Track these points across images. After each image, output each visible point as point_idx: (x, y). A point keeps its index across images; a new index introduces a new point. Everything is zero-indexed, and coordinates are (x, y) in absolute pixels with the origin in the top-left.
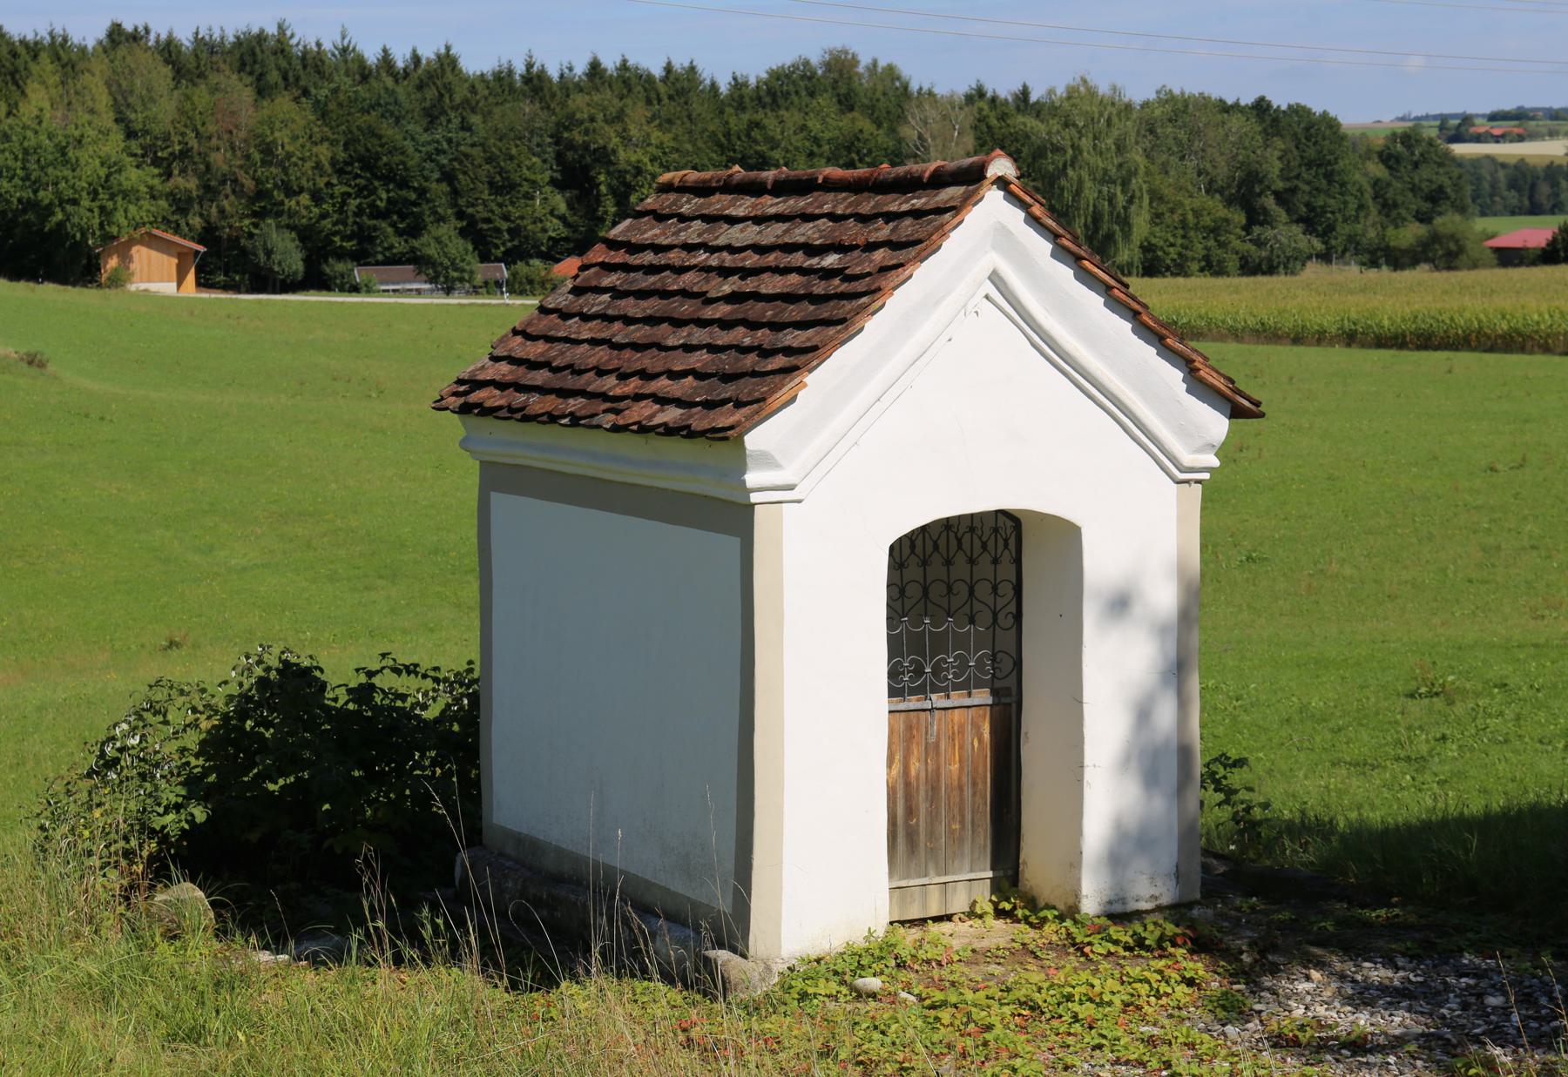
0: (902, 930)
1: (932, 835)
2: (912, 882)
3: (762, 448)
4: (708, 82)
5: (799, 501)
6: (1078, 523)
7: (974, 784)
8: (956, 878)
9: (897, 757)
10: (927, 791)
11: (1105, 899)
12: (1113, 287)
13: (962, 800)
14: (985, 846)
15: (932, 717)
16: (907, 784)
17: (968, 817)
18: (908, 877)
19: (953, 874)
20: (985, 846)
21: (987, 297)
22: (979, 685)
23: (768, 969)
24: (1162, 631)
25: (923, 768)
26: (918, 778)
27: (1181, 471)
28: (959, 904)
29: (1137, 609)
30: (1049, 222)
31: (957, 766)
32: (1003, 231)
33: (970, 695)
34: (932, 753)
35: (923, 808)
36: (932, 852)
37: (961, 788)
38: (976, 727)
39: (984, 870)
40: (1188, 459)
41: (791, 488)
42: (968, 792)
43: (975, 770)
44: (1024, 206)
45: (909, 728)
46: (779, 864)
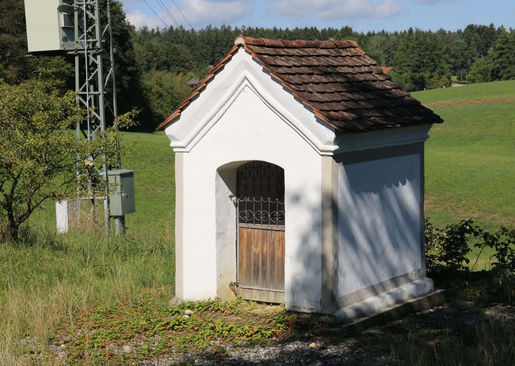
1: (272, 273)
2: (263, 289)
4: (386, 33)
5: (188, 152)
6: (283, 168)
16: (263, 255)
18: (263, 287)
19: (280, 289)
21: (247, 85)
24: (314, 210)
25: (269, 250)
27: (321, 152)
29: (303, 201)
31: (281, 251)
32: (245, 62)
34: (272, 246)
35: (268, 264)
40: (322, 146)
41: (184, 148)
45: (263, 235)
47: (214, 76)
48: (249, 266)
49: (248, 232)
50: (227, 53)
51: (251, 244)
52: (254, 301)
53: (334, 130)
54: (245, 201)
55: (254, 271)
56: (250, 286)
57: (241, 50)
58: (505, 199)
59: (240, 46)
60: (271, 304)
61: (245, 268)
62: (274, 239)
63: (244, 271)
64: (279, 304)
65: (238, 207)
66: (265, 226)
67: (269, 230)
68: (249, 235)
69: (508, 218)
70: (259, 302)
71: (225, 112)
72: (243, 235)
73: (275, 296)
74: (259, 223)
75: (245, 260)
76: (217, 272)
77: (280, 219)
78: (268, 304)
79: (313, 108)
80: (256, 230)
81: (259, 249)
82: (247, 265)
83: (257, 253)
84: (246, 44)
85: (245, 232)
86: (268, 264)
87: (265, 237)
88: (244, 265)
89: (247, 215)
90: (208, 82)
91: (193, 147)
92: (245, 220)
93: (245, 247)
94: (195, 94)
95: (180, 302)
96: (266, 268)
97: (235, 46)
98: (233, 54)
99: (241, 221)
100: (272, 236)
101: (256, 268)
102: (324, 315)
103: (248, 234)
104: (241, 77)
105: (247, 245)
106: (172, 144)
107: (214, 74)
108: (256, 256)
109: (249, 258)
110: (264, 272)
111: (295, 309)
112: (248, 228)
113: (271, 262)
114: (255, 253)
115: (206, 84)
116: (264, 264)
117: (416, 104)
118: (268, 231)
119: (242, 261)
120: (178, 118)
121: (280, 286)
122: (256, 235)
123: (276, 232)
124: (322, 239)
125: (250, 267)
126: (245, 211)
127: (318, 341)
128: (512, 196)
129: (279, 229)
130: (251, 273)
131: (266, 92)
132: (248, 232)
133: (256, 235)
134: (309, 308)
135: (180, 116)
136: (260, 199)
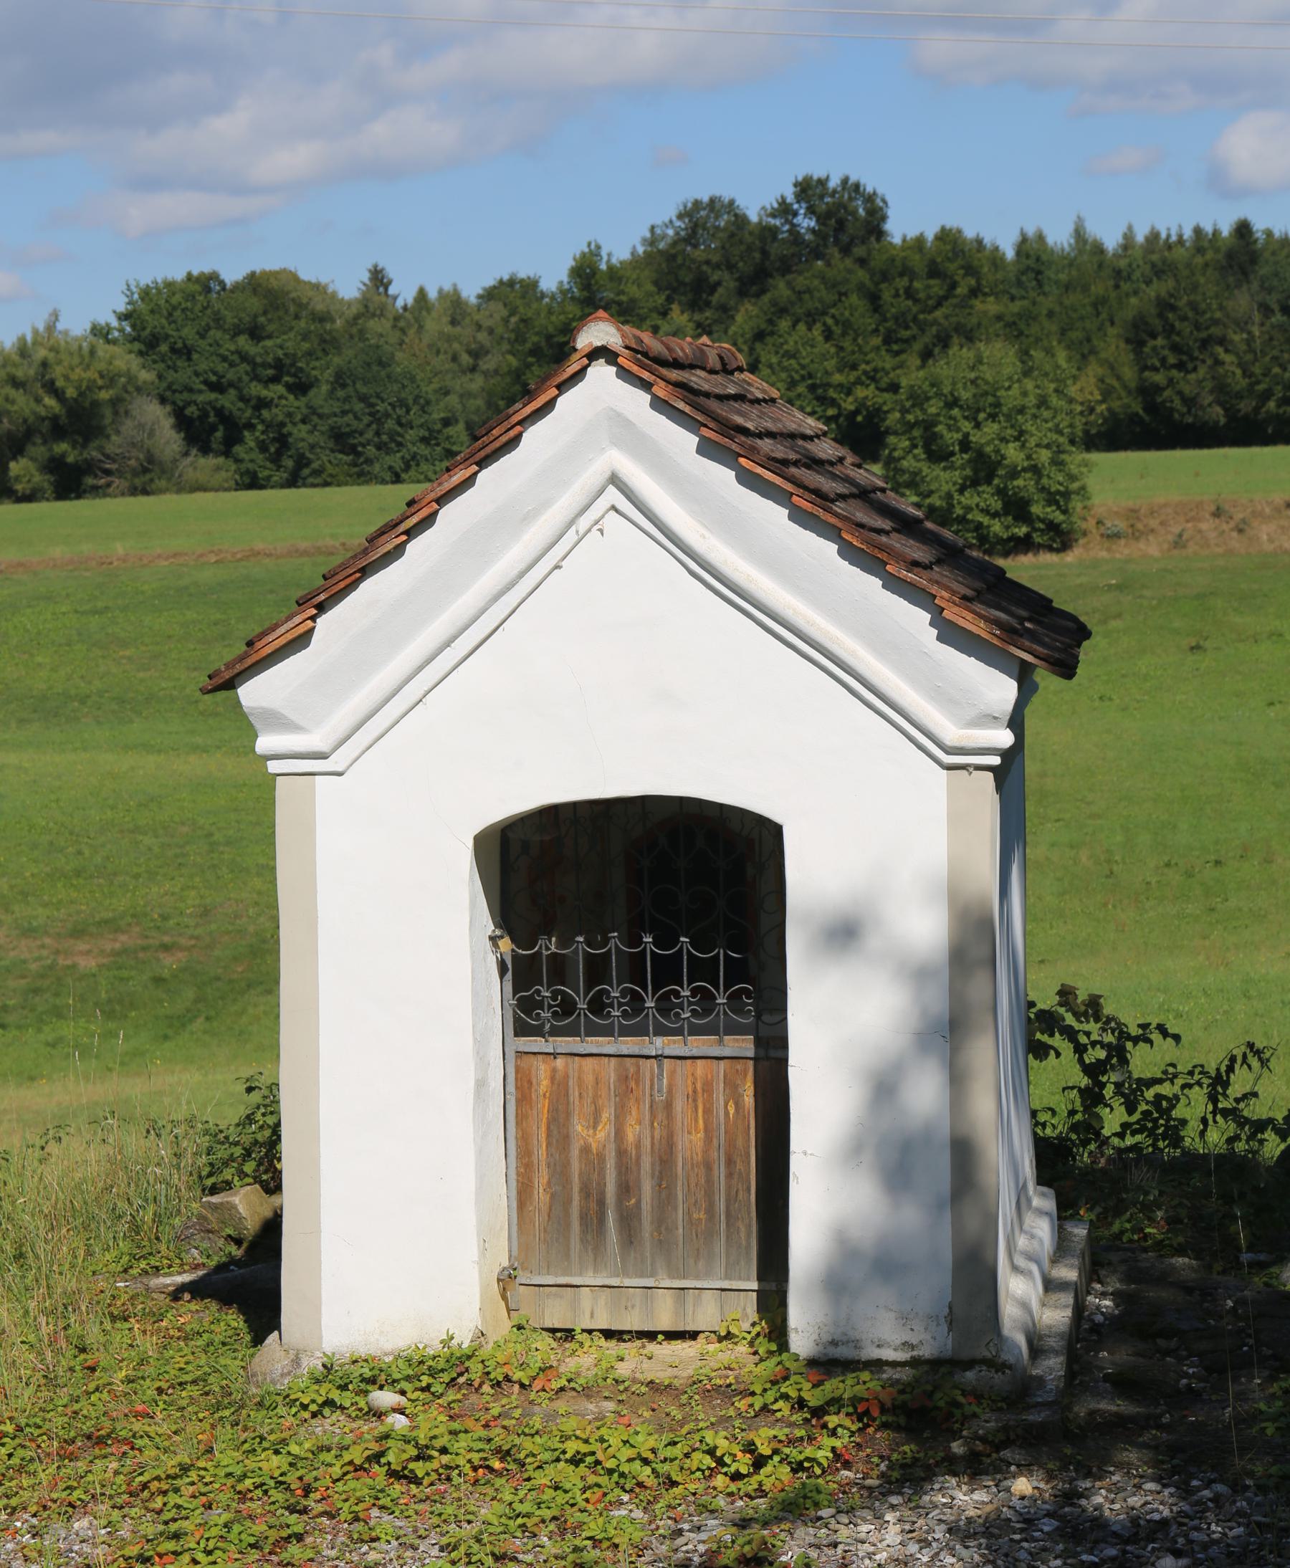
0: (602, 1342)
1: (662, 1220)
2: (627, 1282)
3: (264, 704)
5: (340, 774)
6: (777, 818)
7: (730, 1162)
8: (699, 1284)
9: (605, 1116)
10: (653, 1164)
11: (826, 1338)
12: (792, 494)
13: (709, 1181)
14: (748, 1247)
15: (660, 1067)
16: (621, 1153)
17: (721, 1206)
18: (626, 1274)
19: (697, 1277)
20: (748, 1247)
21: (614, 508)
22: (733, 1030)
23: (297, 1362)
24: (920, 975)
25: (648, 1133)
26: (638, 1146)
27: (948, 753)
28: (706, 1315)
30: (681, 405)
31: (701, 1135)
33: (721, 1042)
34: (661, 1116)
35: (647, 1188)
36: (663, 1244)
37: (708, 1166)
38: (732, 1088)
39: (748, 1279)
40: (953, 733)
41: (322, 756)
42: (720, 1172)
43: (731, 1143)
44: (646, 386)
45: (624, 1079)
46: (316, 1232)
47: (476, 474)
48: (559, 1200)
49: (554, 1070)
50: (544, 379)
51: (568, 1115)
52: (590, 1332)
53: (1016, 670)
54: (539, 953)
55: (584, 1217)
56: (566, 1273)
57: (601, 373)
58: (14, 882)
59: (598, 353)
60: (660, 1337)
61: (545, 1209)
62: (670, 1091)
63: (538, 1220)
64: (693, 1335)
65: (509, 975)
66: (628, 1045)
67: (648, 1057)
68: (560, 1086)
69: (39, 943)
70: (608, 1334)
71: (513, 611)
72: (530, 1082)
73: (680, 1302)
74: (607, 1032)
75: (541, 1178)
76: (478, 1235)
77: (625, 1015)
78: (651, 1336)
79: (934, 589)
80: (589, 1060)
81: (603, 1134)
82: (553, 1196)
83: (594, 1146)
84: (627, 347)
85: (541, 1070)
86: (647, 1188)
87: (633, 1084)
88: (541, 1195)
89: (550, 1007)
90: (442, 500)
91: (364, 752)
92: (543, 1025)
93: (543, 1128)
94: (389, 547)
95: (313, 1363)
96: (639, 1202)
97: (575, 356)
98: (562, 387)
99: (522, 1029)
100: (660, 1080)
101: (593, 1206)
102: (970, 1364)
103: (552, 1079)
104: (594, 473)
105: (552, 1121)
106: (265, 743)
107: (477, 464)
108: (593, 1160)
109: (560, 1171)
110: (629, 1222)
111: (843, 1352)
112: (555, 1055)
113: (661, 1178)
114: (586, 1150)
115: (436, 506)
116: (626, 1189)
117: (1002, 572)
118: (642, 1061)
119: (530, 1180)
120: (303, 640)
121: (701, 1264)
122: (589, 1079)
123: (679, 1062)
124: (957, 1080)
125: (567, 1203)
126: (538, 992)
127: (1013, 1468)
128: (36, 871)
129: (695, 1052)
130: (568, 1225)
131: (707, 534)
132: (554, 1070)
133: (589, 1079)
134: (898, 1342)
135: (311, 631)
136: (606, 941)
